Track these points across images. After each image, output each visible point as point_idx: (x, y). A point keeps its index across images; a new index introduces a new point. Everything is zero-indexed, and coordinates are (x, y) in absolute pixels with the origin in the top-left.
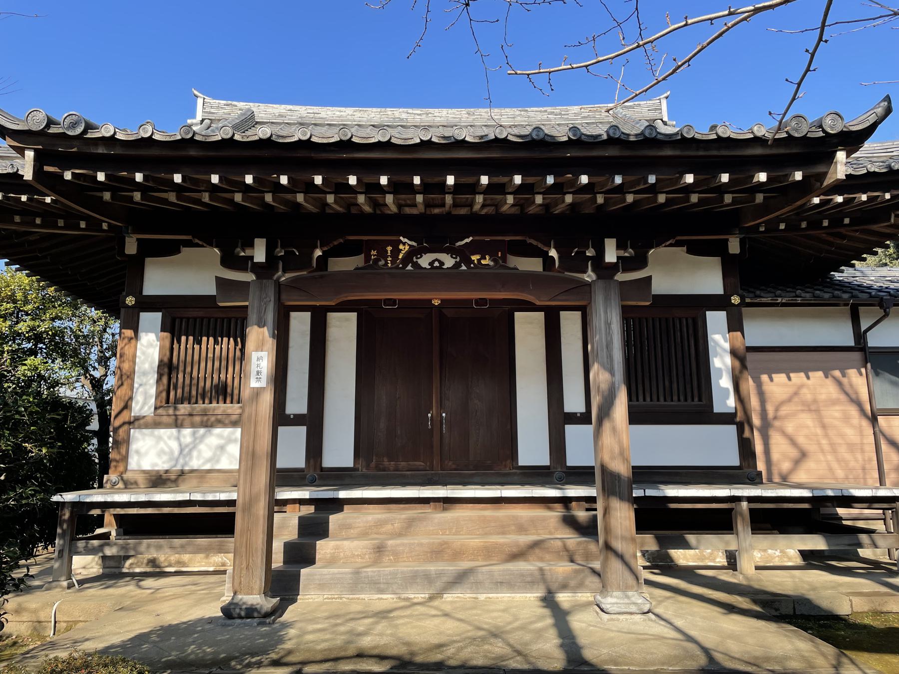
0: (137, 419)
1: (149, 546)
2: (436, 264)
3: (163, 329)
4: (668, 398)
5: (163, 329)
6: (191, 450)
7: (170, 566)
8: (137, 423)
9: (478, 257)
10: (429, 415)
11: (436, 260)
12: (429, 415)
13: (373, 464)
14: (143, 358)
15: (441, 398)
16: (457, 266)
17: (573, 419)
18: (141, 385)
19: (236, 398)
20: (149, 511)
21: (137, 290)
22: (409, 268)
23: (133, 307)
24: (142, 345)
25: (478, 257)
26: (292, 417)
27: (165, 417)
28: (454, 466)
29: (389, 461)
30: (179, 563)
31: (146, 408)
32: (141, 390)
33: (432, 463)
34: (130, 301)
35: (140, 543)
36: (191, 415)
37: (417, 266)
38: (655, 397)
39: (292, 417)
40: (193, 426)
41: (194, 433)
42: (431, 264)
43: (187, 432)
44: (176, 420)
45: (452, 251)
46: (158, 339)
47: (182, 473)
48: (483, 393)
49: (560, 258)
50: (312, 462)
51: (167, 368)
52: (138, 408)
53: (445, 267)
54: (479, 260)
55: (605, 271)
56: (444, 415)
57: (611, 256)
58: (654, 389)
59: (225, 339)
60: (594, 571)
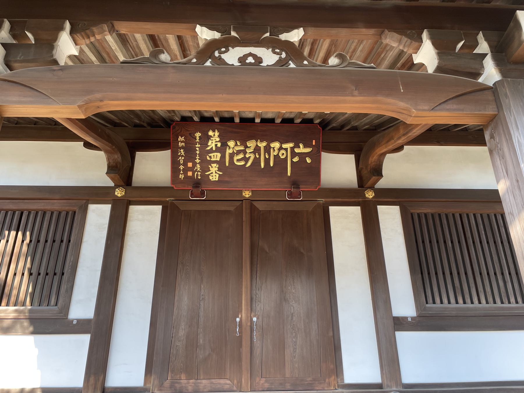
2: (250, 60)
4: (505, 300)
9: (291, 145)
10: (238, 320)
11: (250, 54)
12: (238, 320)
13: (167, 383)
15: (252, 299)
16: (281, 63)
17: (401, 324)
19: (13, 299)
25: (291, 145)
26: (75, 322)
28: (267, 385)
29: (188, 379)
33: (240, 382)
38: (490, 299)
39: (410, 319)
42: (242, 60)
45: (274, 44)
48: (300, 294)
50: (92, 380)
53: (264, 64)
54: (292, 149)
56: (255, 319)
58: (481, 289)
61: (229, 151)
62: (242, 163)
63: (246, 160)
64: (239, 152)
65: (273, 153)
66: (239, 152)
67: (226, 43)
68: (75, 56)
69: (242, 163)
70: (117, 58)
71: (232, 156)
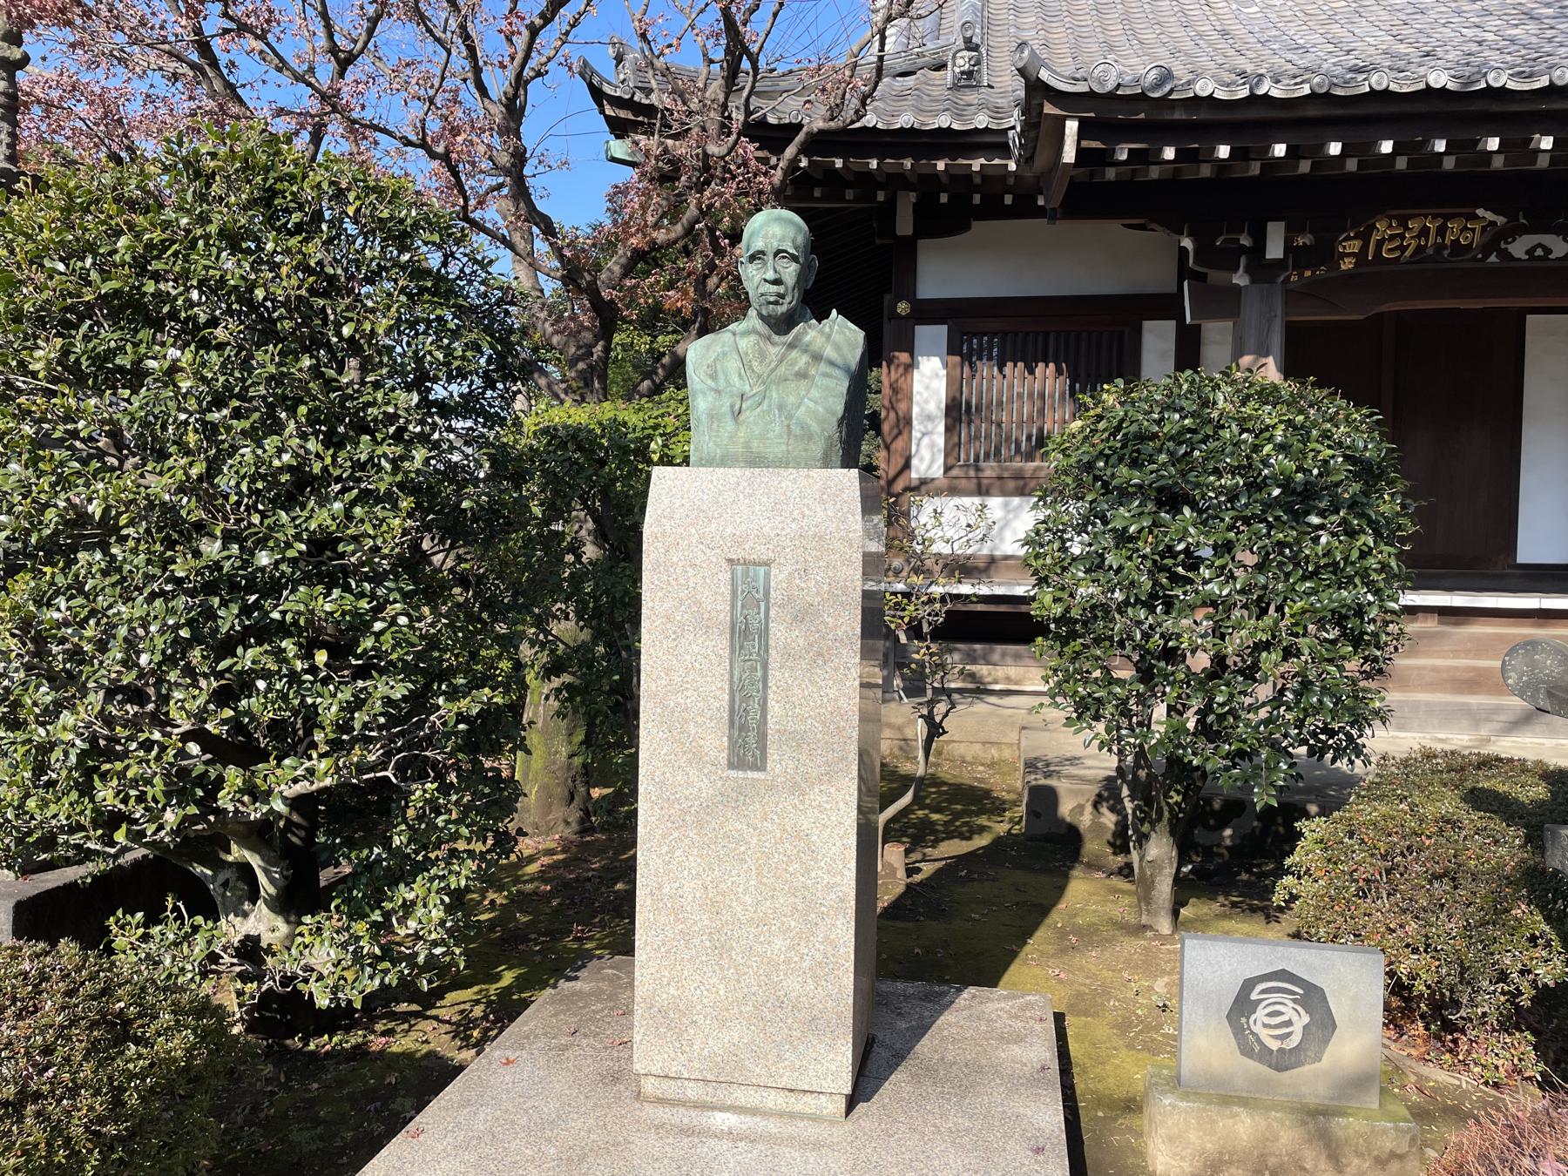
0: (924, 482)
1: (1004, 655)
2: (1539, 252)
3: (951, 352)
5: (951, 352)
6: (1002, 529)
7: (996, 682)
8: (924, 489)
11: (1540, 245)
14: (925, 394)
18: (924, 434)
20: (1003, 608)
21: (909, 294)
22: (1493, 258)
23: (907, 317)
24: (923, 375)
27: (964, 482)
30: (1008, 679)
31: (935, 467)
32: (926, 441)
34: (903, 308)
35: (992, 651)
36: (1000, 478)
37: (1506, 255)
40: (1004, 493)
41: (1006, 505)
42: (1530, 252)
43: (995, 503)
44: (979, 485)
46: (946, 365)
47: (992, 560)
49: (1196, 251)
51: (957, 413)
52: (923, 467)
55: (1262, 270)
57: (1275, 250)
59: (1041, 365)
60: (1281, 692)
61: (1376, 237)
62: (1397, 254)
63: (1403, 249)
64: (1392, 238)
65: (1450, 238)
66: (1392, 238)
67: (1512, 232)
68: (907, 465)
69: (1397, 254)
70: (1489, 670)
71: (1380, 244)
